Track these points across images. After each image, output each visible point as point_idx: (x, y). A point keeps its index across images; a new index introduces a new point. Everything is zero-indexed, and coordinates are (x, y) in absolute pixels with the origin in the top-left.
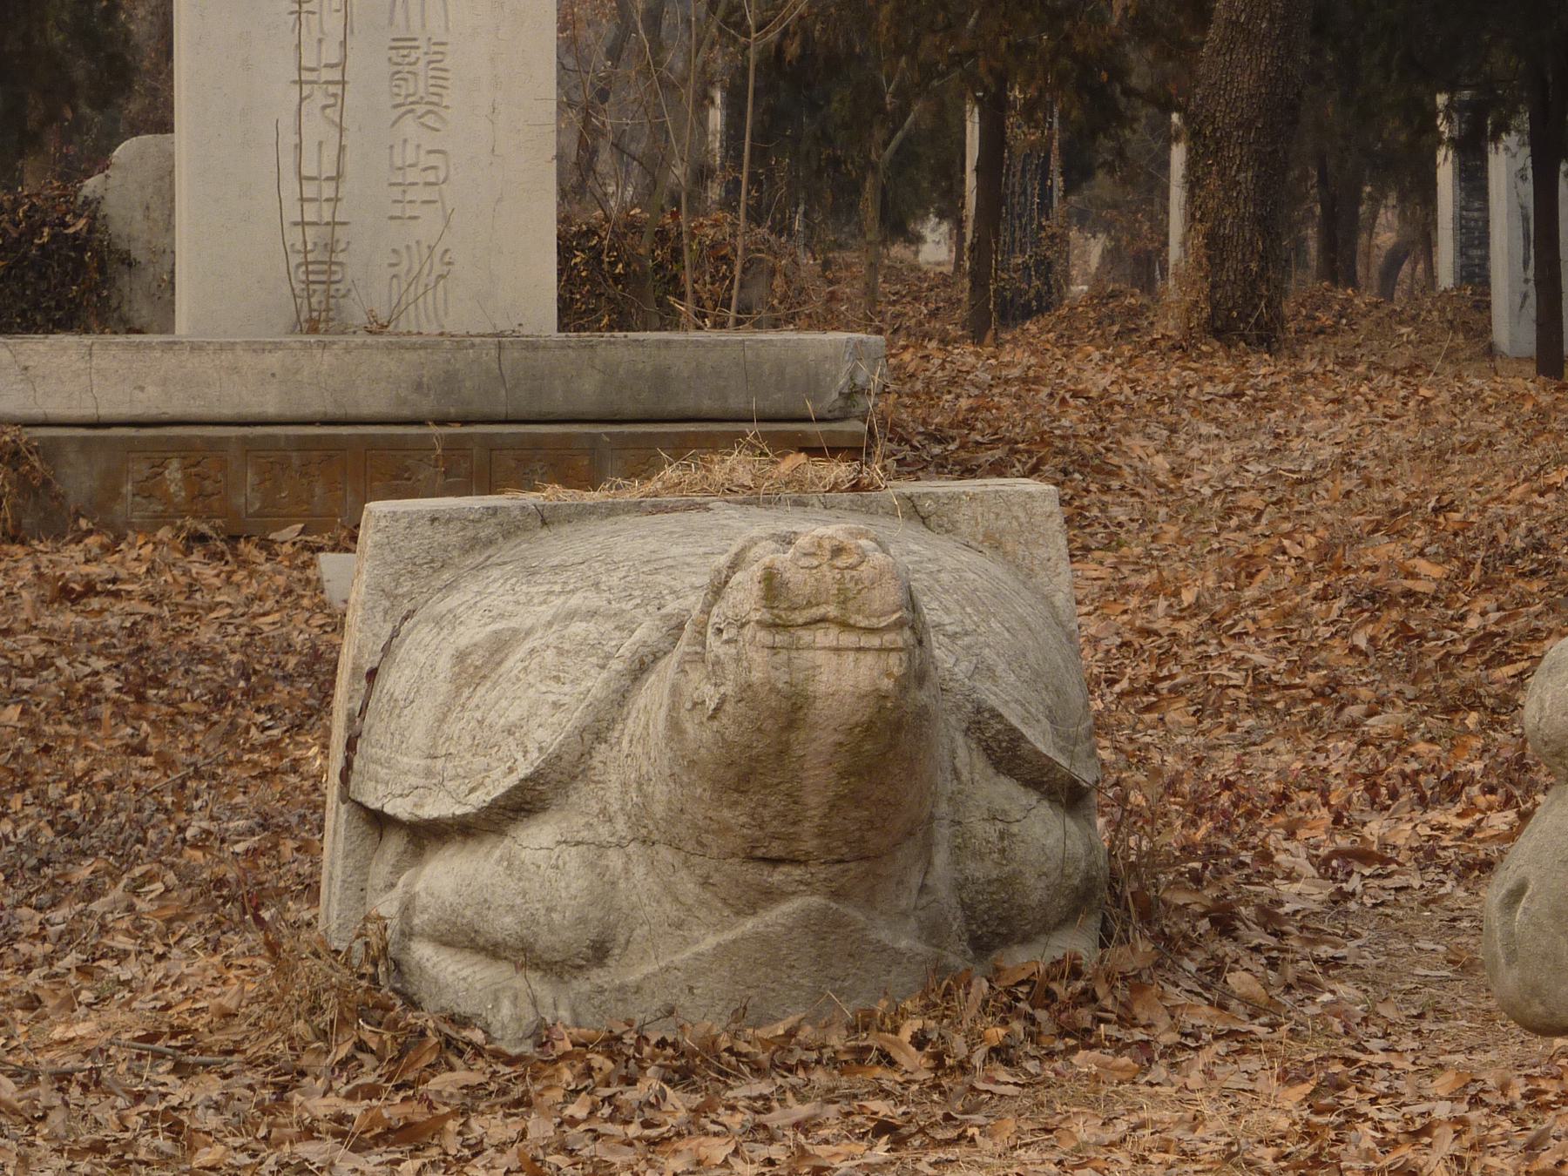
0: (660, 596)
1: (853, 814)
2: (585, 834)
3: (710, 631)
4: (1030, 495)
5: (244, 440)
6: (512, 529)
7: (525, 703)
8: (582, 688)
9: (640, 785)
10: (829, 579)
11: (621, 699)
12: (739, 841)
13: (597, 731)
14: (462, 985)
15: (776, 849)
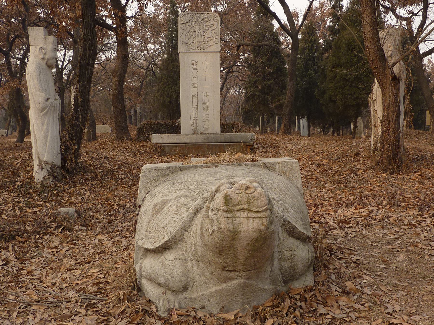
0: (203, 191)
1: (252, 260)
2: (182, 257)
3: (210, 210)
4: (292, 162)
5: (185, 145)
6: (173, 171)
7: (168, 220)
8: (182, 217)
9: (195, 246)
10: (244, 197)
11: (192, 220)
12: (220, 266)
13: (185, 228)
14: (152, 294)
15: (231, 268)
